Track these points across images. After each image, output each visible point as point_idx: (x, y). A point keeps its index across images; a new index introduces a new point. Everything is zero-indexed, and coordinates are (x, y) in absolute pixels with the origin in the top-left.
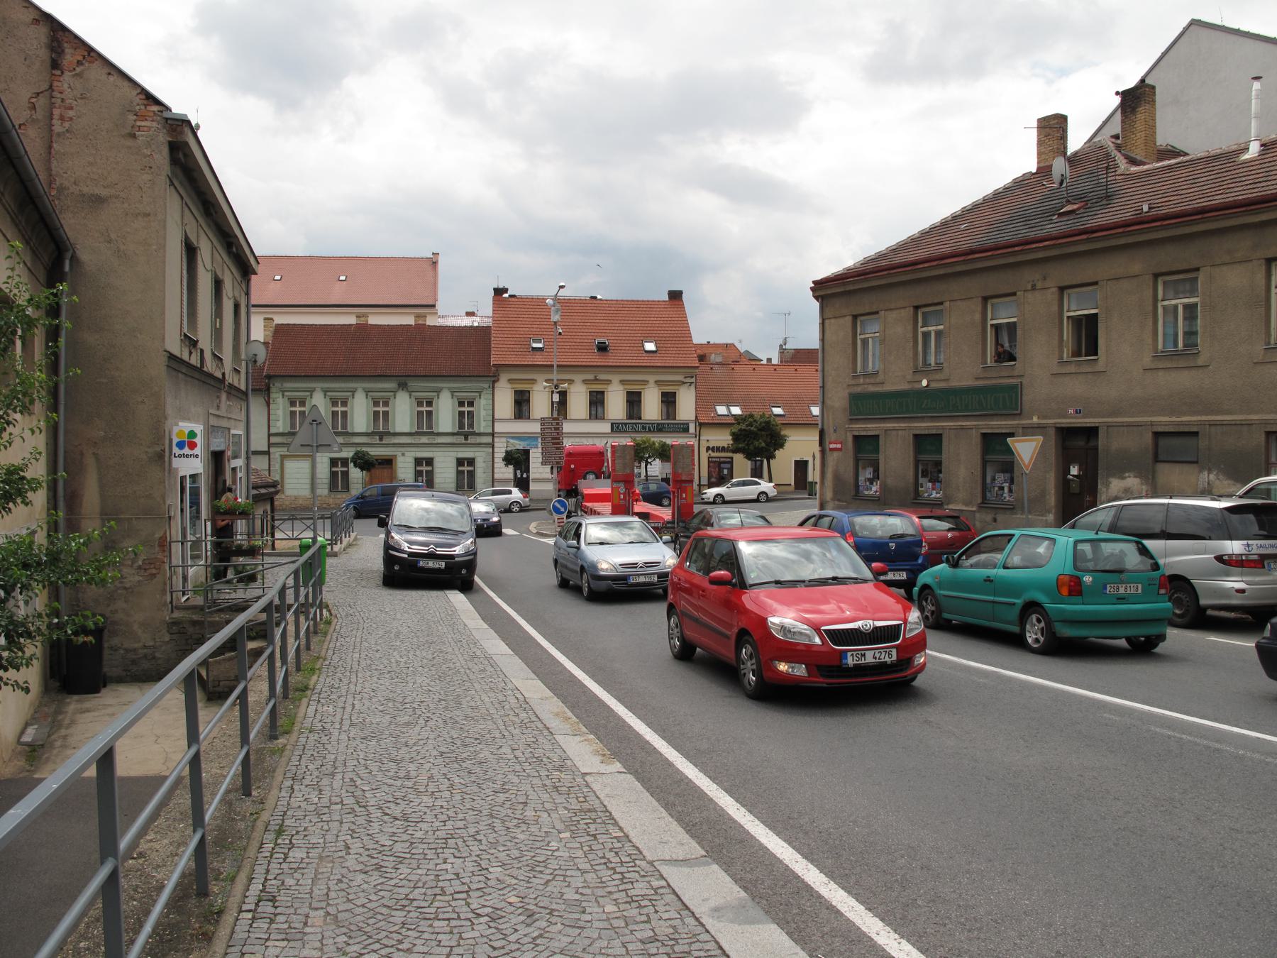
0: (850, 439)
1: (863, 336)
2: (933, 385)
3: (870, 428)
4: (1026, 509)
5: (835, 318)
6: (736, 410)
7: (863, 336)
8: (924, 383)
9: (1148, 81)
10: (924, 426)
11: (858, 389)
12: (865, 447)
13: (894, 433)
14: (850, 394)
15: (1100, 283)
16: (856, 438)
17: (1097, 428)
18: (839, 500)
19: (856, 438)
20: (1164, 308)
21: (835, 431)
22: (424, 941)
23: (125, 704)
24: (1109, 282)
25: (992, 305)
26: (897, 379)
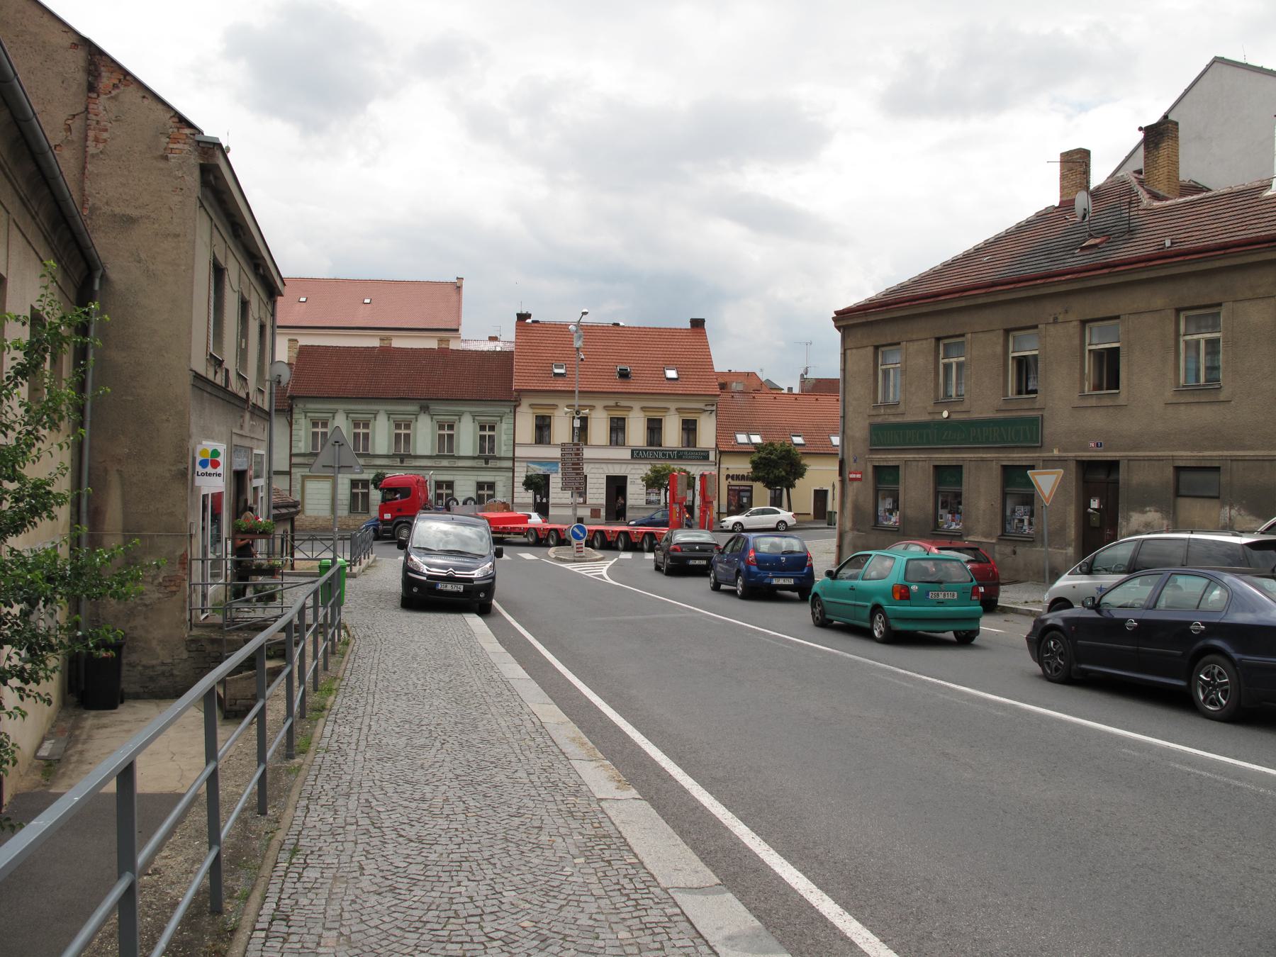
0: (870, 470)
1: (884, 367)
2: (954, 416)
3: (890, 459)
8: (945, 414)
11: (879, 420)
13: (914, 463)
18: (858, 530)
21: (855, 461)
26: (918, 409)
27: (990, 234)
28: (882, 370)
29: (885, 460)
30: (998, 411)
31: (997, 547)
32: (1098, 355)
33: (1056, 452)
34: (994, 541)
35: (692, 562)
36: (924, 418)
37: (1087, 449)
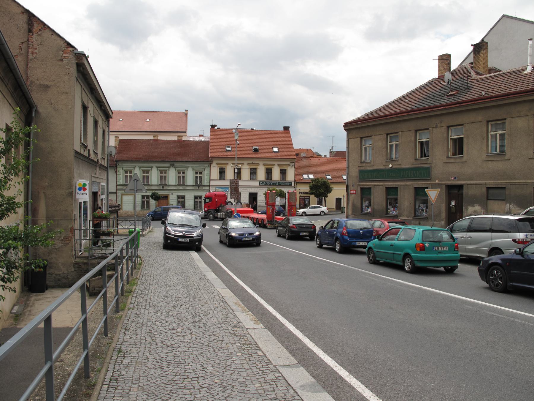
0: (359, 189)
1: (365, 146)
2: (394, 167)
3: (367, 185)
5: (353, 138)
8: (390, 166)
10: (390, 184)
11: (363, 168)
13: (377, 187)
17: (463, 185)
19: (362, 189)
20: (364, 147)
21: (353, 186)
26: (379, 164)
30: (413, 164)
33: (437, 182)
34: (411, 219)
36: (381, 167)
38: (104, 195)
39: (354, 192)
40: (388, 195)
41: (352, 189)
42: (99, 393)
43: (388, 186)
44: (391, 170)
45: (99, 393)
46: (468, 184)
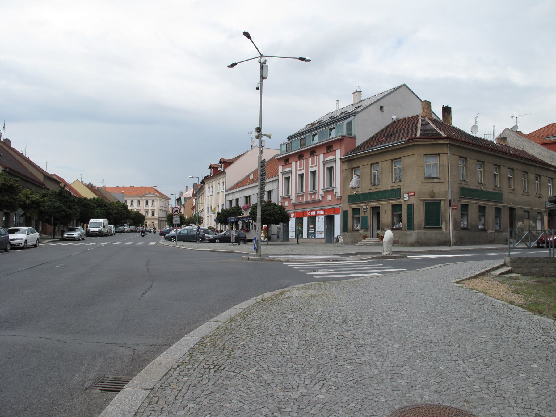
0: (460, 205)
1: (395, 168)
2: (358, 193)
3: (466, 201)
4: (513, 238)
5: (453, 155)
6: (4, 217)
7: (395, 168)
8: (355, 192)
9: (5, 138)
10: (482, 203)
11: (462, 186)
12: (464, 208)
13: (473, 204)
14: (459, 187)
15: (440, 155)
16: (462, 205)
17: (515, 208)
18: (456, 230)
19: (462, 205)
20: (394, 169)
21: (454, 201)
22: (236, 373)
23: (150, 287)
24: (404, 158)
25: (394, 162)
26: (366, 188)
27: (383, 127)
28: (394, 169)
29: (465, 202)
30: (494, 190)
31: (495, 233)
32: (285, 178)
33: (505, 204)
34: (494, 231)
35: (291, 265)
36: (475, 188)
37: (510, 204)
38: (299, 175)
39: (456, 207)
40: (394, 212)
41: (453, 205)
42: (482, 405)
43: (480, 205)
44: (481, 191)
45: (482, 405)
46: (518, 208)
